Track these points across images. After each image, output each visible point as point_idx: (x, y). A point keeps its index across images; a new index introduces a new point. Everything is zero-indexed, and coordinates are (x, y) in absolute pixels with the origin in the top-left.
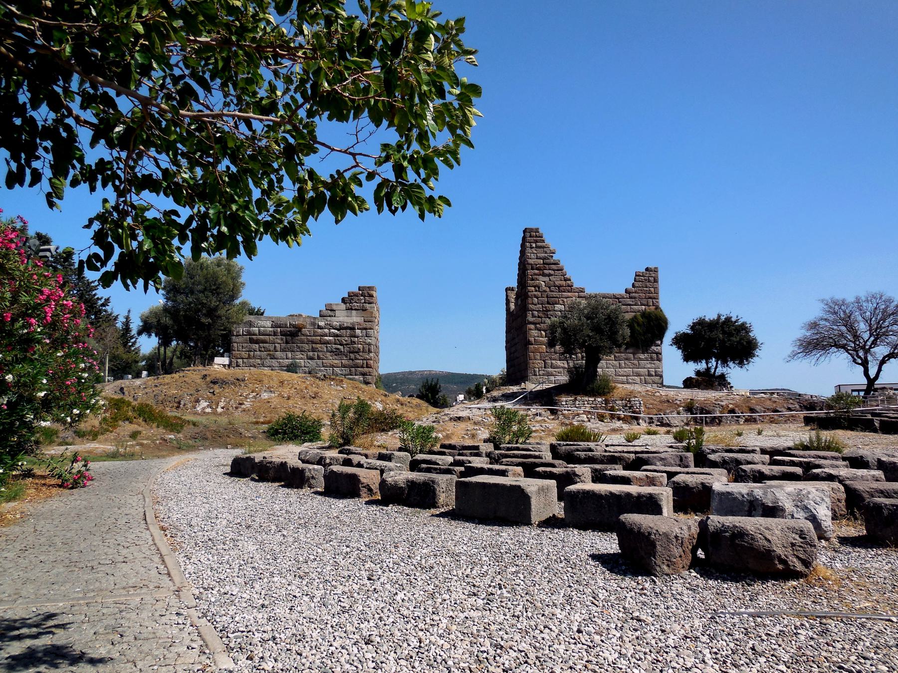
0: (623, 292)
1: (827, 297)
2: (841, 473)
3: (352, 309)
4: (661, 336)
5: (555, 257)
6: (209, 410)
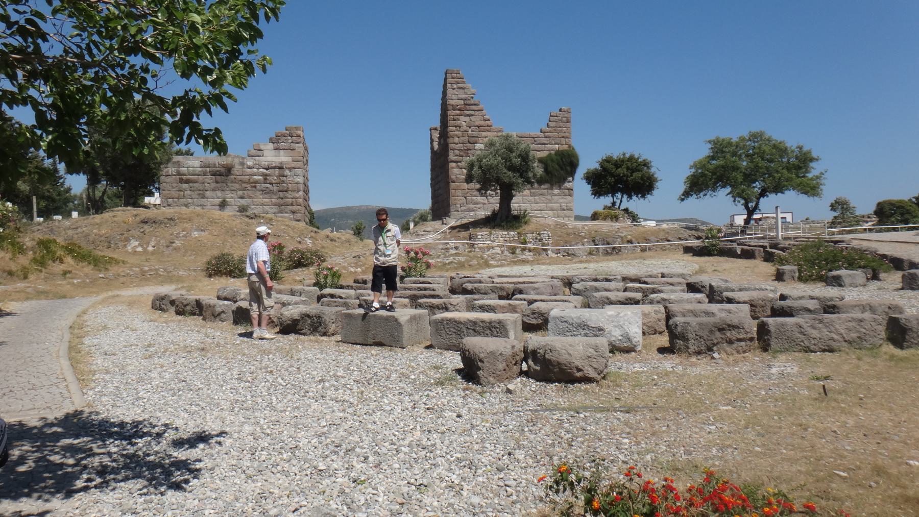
1: (713, 138)
2: (672, 297)
4: (572, 173)
6: (140, 249)
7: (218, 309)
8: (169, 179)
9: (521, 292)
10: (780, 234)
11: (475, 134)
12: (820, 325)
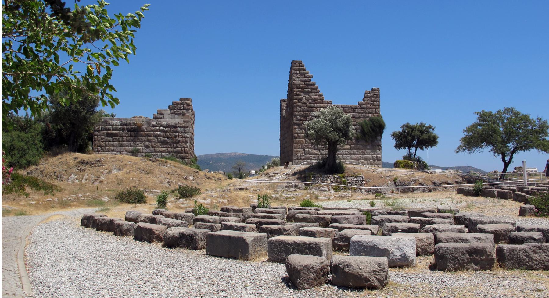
0: (357, 105)
1: (480, 111)
2: (441, 227)
3: (174, 113)
5: (313, 80)
7: (125, 227)
8: (100, 133)
9: (336, 221)
10: (526, 180)
12: (540, 251)
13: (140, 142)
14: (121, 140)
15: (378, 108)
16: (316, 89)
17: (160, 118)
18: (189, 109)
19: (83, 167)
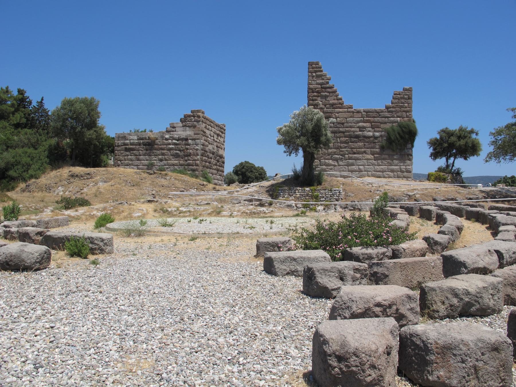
5: (331, 83)
8: (119, 148)
11: (329, 110)
13: (155, 155)
14: (137, 154)
15: (410, 111)
16: (335, 92)
17: (173, 131)
18: (199, 121)
19: (72, 180)
